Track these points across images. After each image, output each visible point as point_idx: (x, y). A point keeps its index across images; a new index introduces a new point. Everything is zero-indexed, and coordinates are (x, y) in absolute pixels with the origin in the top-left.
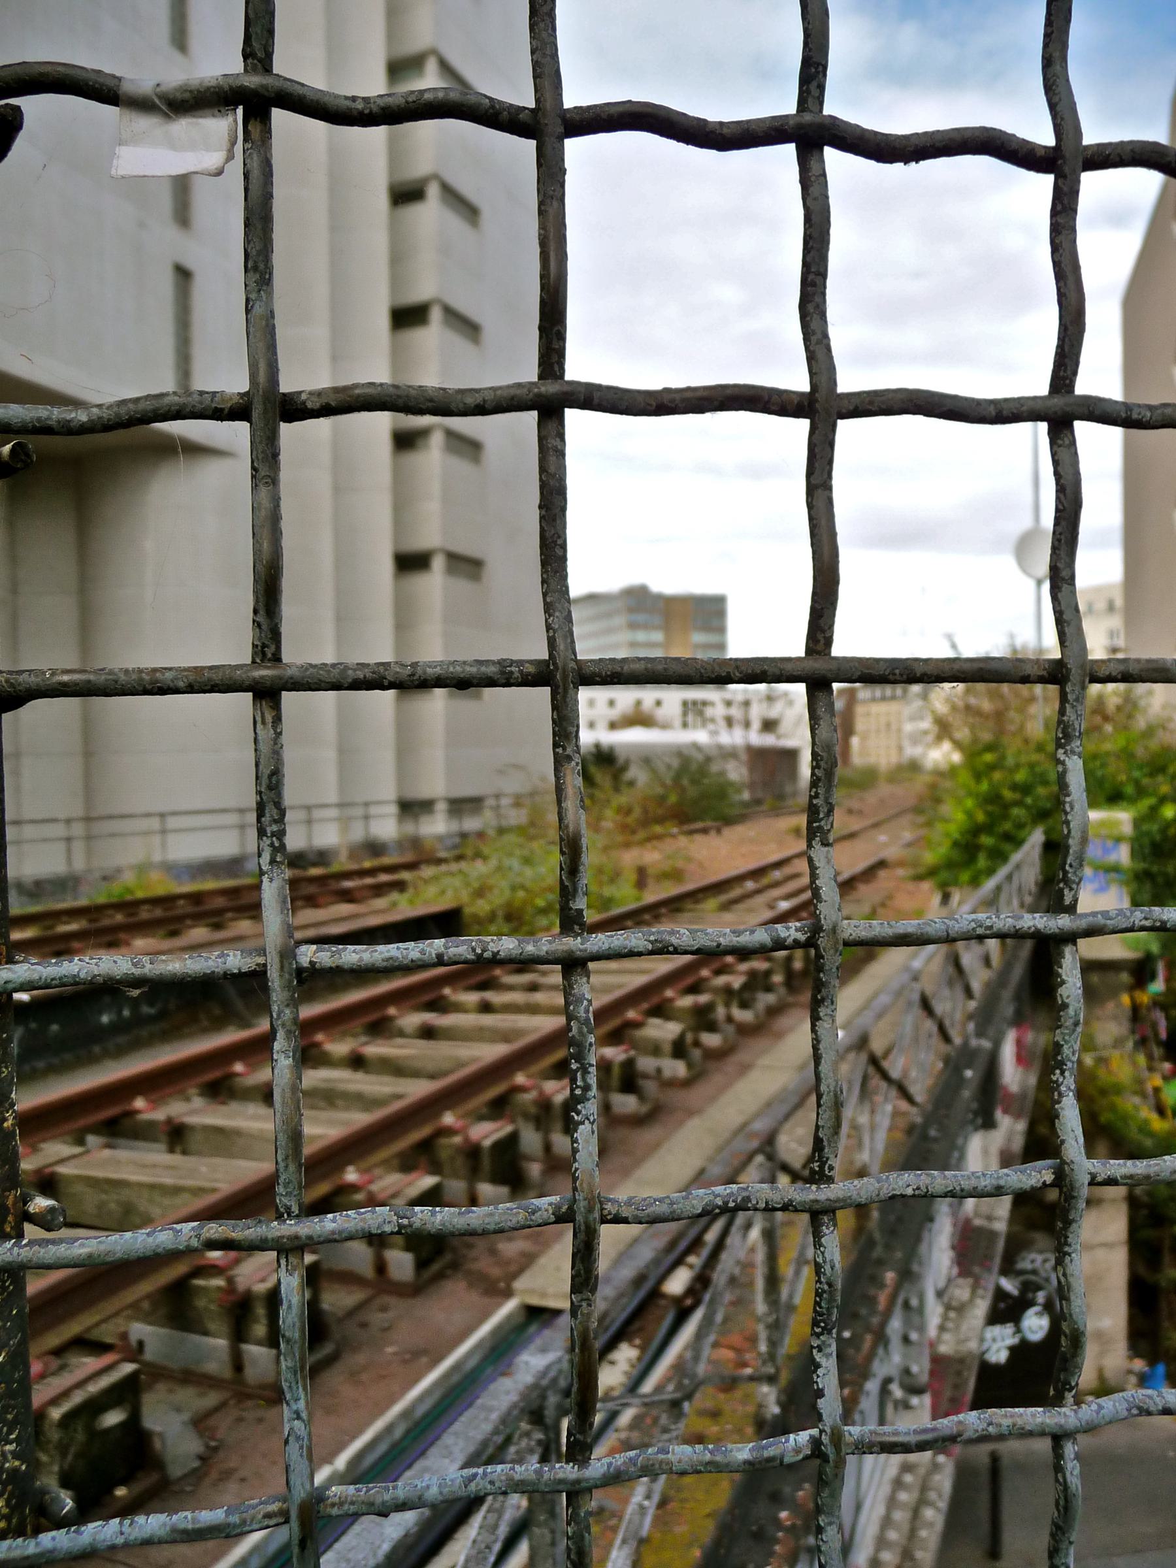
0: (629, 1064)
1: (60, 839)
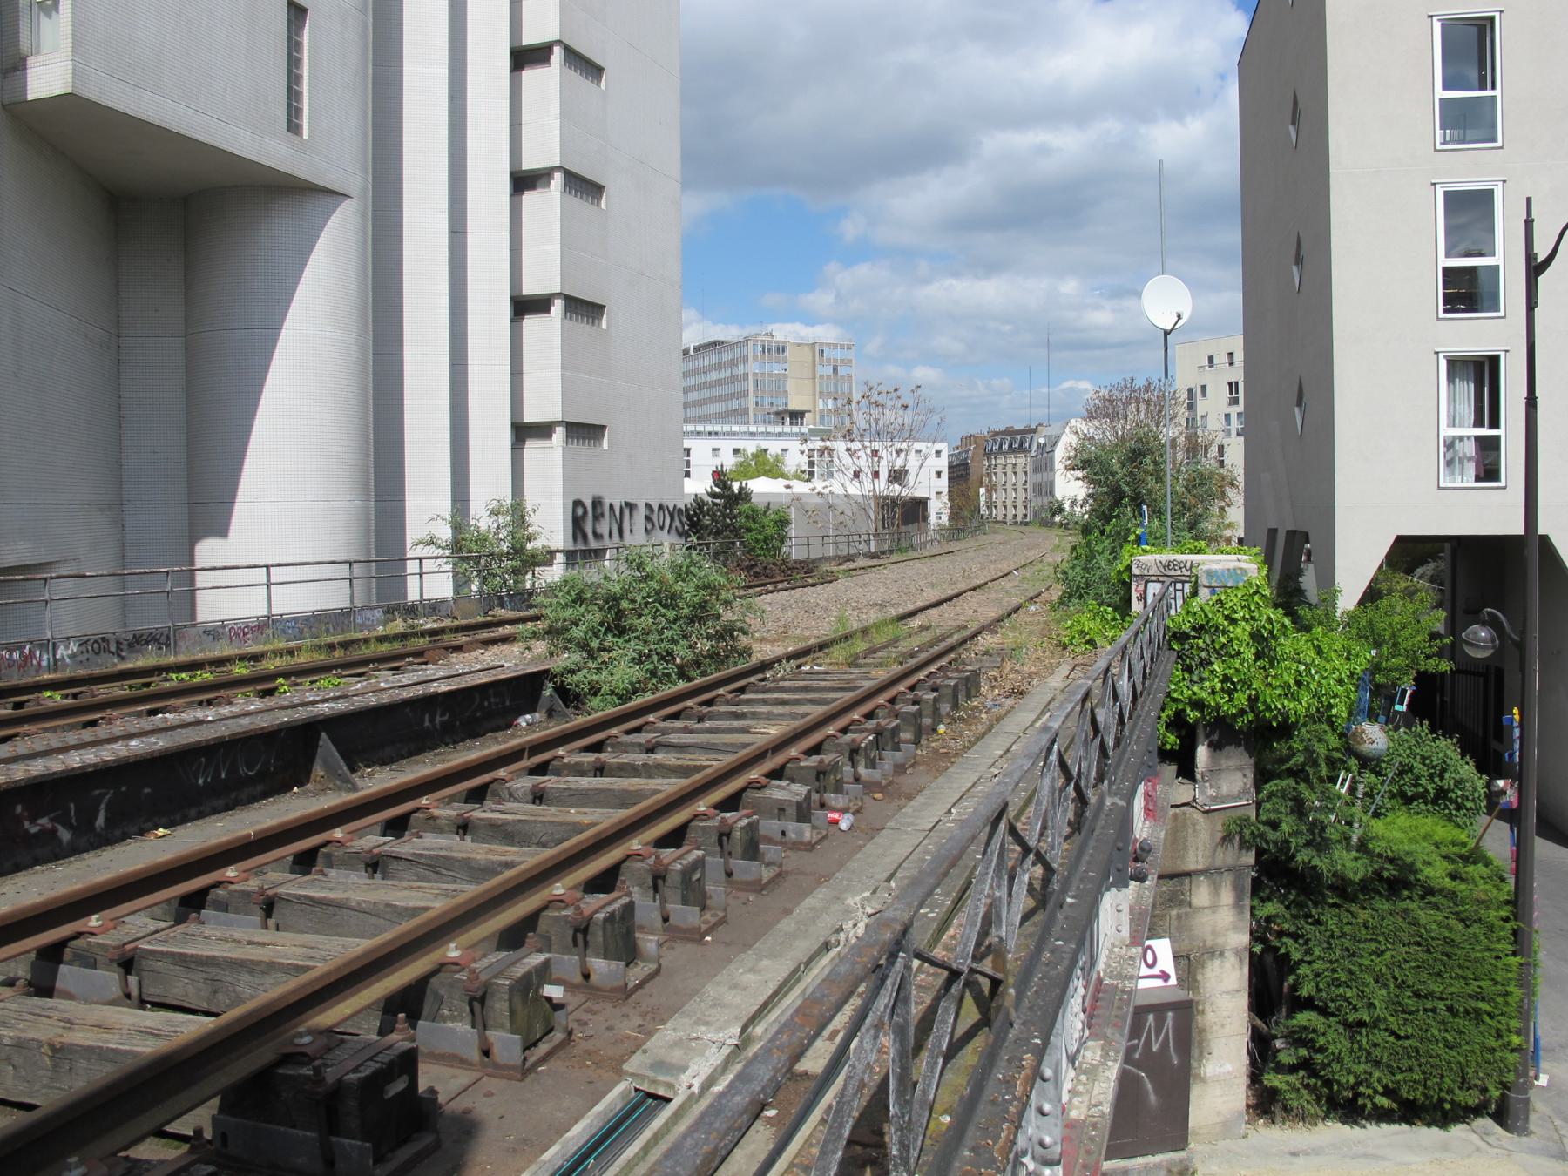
0: (752, 827)
1: (345, 562)
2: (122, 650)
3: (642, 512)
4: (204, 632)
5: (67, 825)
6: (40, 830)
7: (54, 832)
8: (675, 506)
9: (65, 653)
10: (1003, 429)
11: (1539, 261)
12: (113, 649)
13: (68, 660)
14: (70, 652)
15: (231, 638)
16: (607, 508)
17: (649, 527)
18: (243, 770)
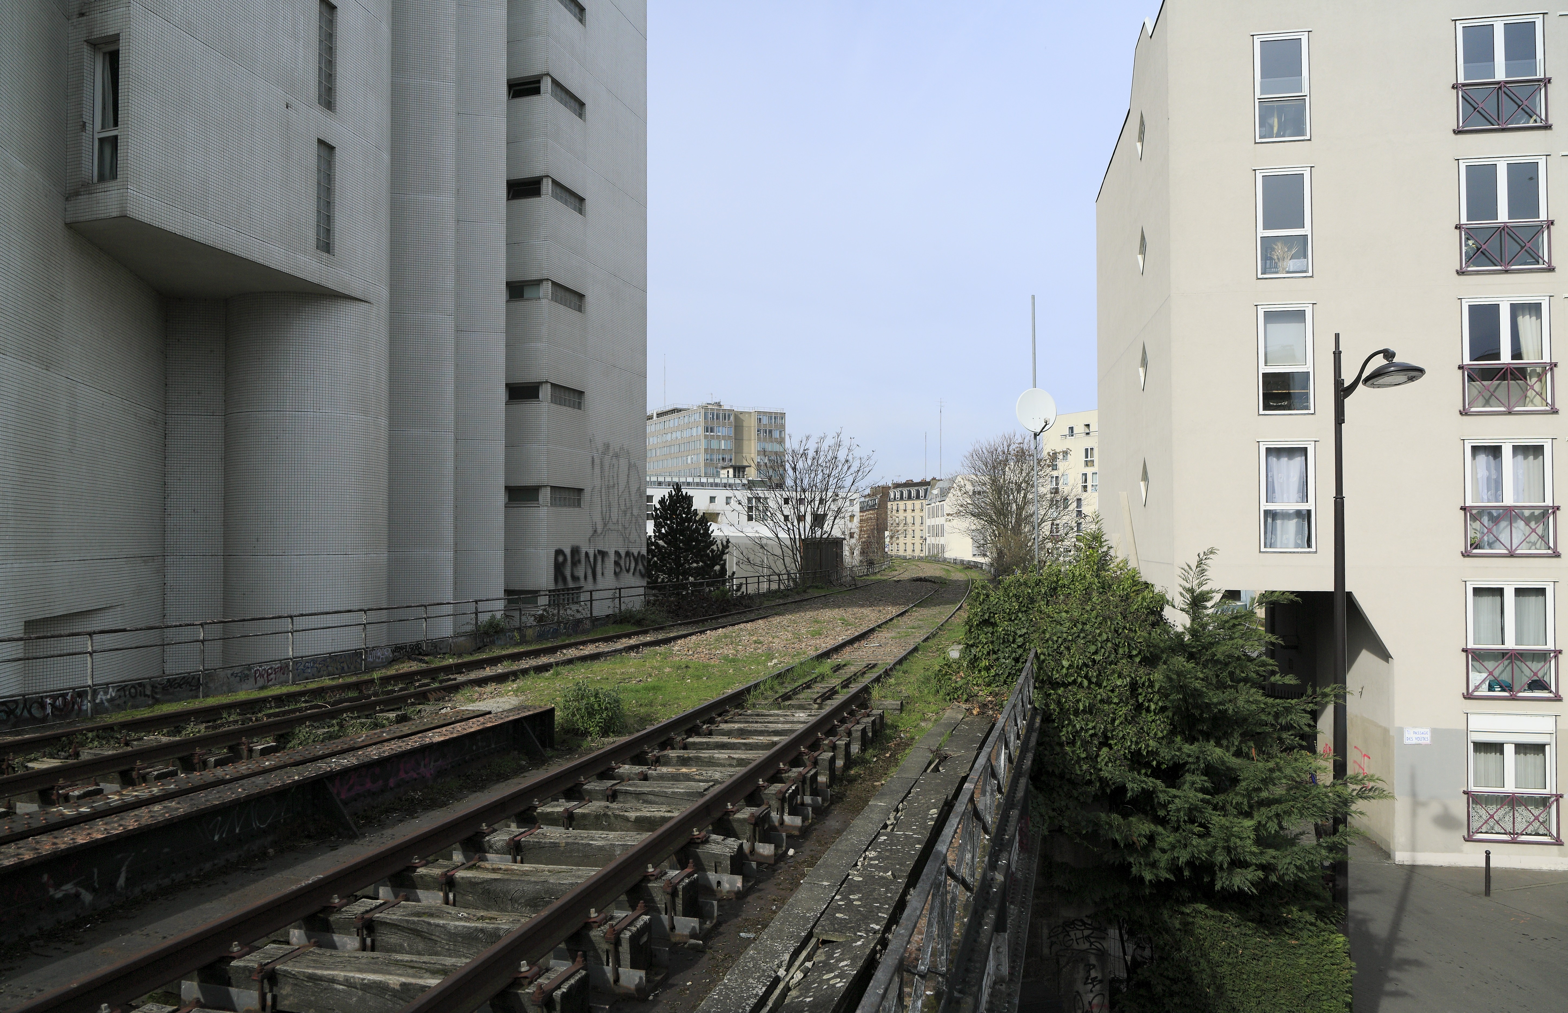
2: (156, 693)
3: (612, 557)
4: (232, 674)
5: (93, 890)
6: (64, 895)
7: (77, 895)
8: (639, 553)
9: (104, 698)
10: (904, 481)
11: (1345, 386)
12: (148, 692)
13: (106, 704)
14: (109, 697)
15: (256, 679)
16: (583, 555)
17: (618, 570)
18: (256, 824)
